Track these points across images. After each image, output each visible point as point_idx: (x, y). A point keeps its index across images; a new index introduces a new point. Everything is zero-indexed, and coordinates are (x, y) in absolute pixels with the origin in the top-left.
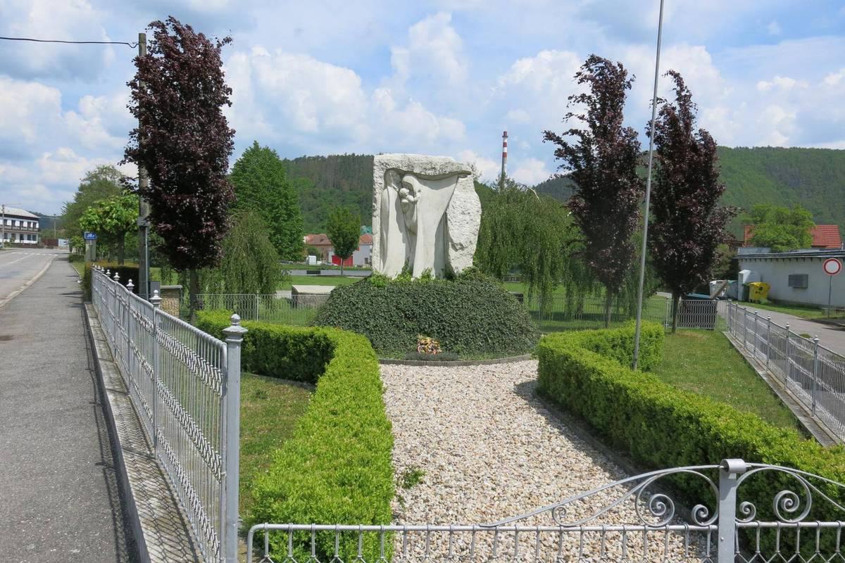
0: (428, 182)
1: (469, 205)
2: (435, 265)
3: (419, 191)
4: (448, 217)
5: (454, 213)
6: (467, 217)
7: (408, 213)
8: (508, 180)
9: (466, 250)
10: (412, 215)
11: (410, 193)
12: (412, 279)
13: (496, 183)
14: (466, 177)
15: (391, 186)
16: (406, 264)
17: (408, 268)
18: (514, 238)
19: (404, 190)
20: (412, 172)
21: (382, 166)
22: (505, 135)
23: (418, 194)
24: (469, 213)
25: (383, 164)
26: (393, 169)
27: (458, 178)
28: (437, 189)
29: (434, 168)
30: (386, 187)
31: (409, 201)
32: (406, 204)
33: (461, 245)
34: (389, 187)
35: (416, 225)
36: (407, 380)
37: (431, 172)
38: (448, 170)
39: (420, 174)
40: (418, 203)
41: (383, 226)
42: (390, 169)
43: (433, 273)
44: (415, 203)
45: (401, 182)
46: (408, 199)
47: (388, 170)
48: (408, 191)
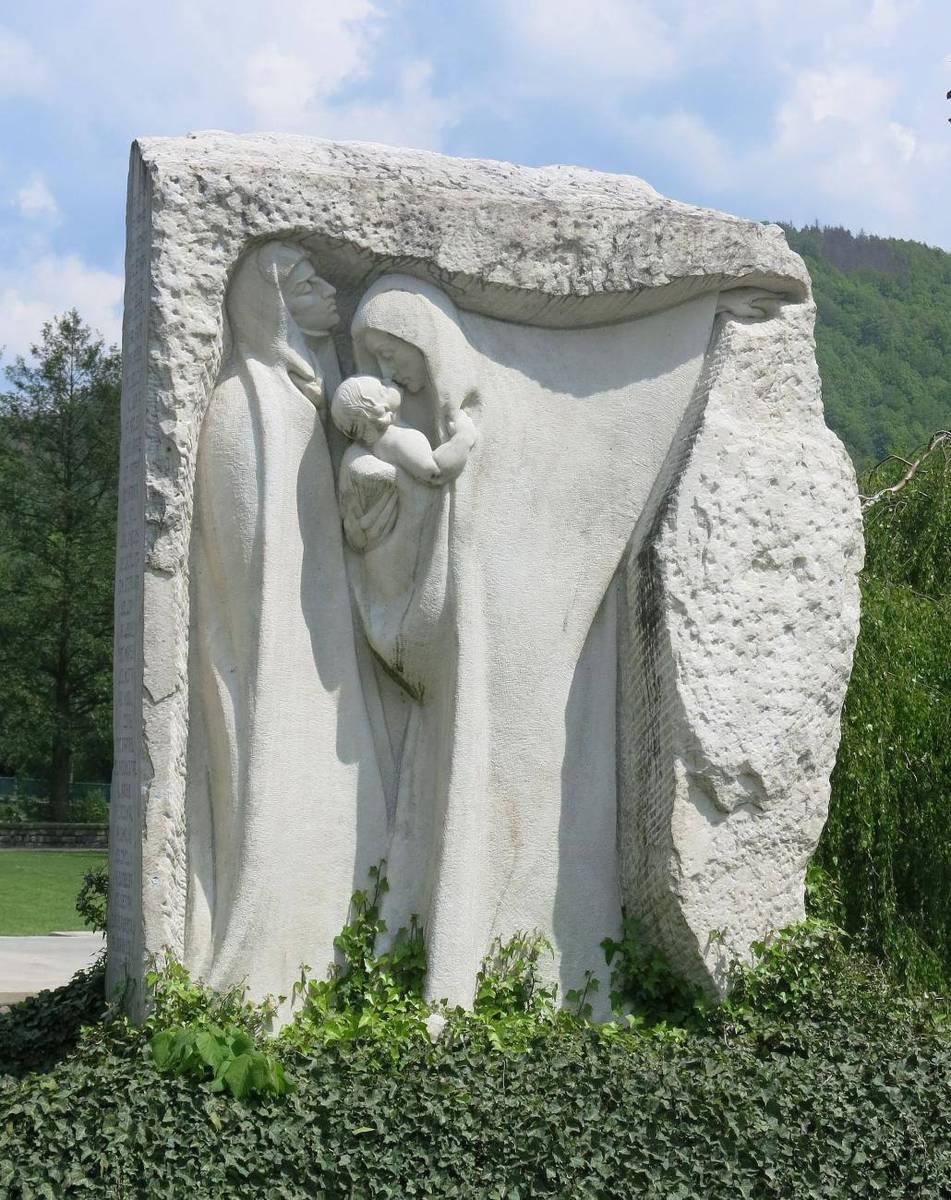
0: (521, 337)
1: (802, 504)
2: (565, 915)
3: (472, 400)
4: (672, 584)
5: (705, 556)
6: (788, 590)
7: (384, 557)
8: (93, 353)
9: (774, 809)
10: (417, 569)
11: (405, 417)
12: (435, 1024)
13: (35, 364)
14: (766, 315)
15: (270, 358)
16: (367, 910)
17: (383, 944)
18: (29, 1049)
19: (368, 391)
20: (430, 262)
21: (219, 215)
23: (464, 421)
24: (799, 562)
25: (220, 199)
26: (294, 238)
28: (582, 392)
29: (574, 245)
30: (232, 363)
31: (406, 467)
32: (375, 488)
33: (750, 776)
34: (254, 365)
35: (444, 633)
38: (666, 265)
39: (480, 281)
40: (463, 483)
41: (209, 640)
42: (269, 239)
43: (549, 972)
44: (441, 481)
46: (395, 455)
47: (257, 243)
48: (394, 395)
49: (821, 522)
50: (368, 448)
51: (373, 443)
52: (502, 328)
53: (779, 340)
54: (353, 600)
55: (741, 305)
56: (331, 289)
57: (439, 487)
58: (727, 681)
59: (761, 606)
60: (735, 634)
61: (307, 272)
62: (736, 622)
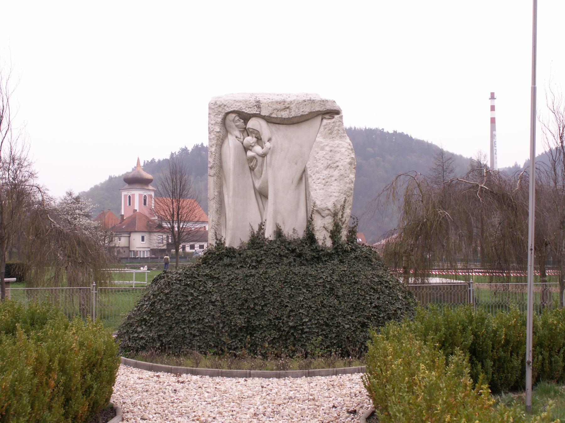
3: (269, 140)
20: (260, 114)
22: (492, 97)
23: (268, 145)
27: (322, 119)
36: (149, 403)
37: (285, 114)
45: (245, 128)
49: (343, 158)
50: (251, 150)
51: (185, 147)
52: (277, 125)
53: (333, 123)
54: (252, 180)
55: (327, 116)
56: (243, 121)
57: (264, 157)
58: (321, 191)
59: (329, 176)
60: (324, 182)
61: (237, 118)
62: (324, 179)
